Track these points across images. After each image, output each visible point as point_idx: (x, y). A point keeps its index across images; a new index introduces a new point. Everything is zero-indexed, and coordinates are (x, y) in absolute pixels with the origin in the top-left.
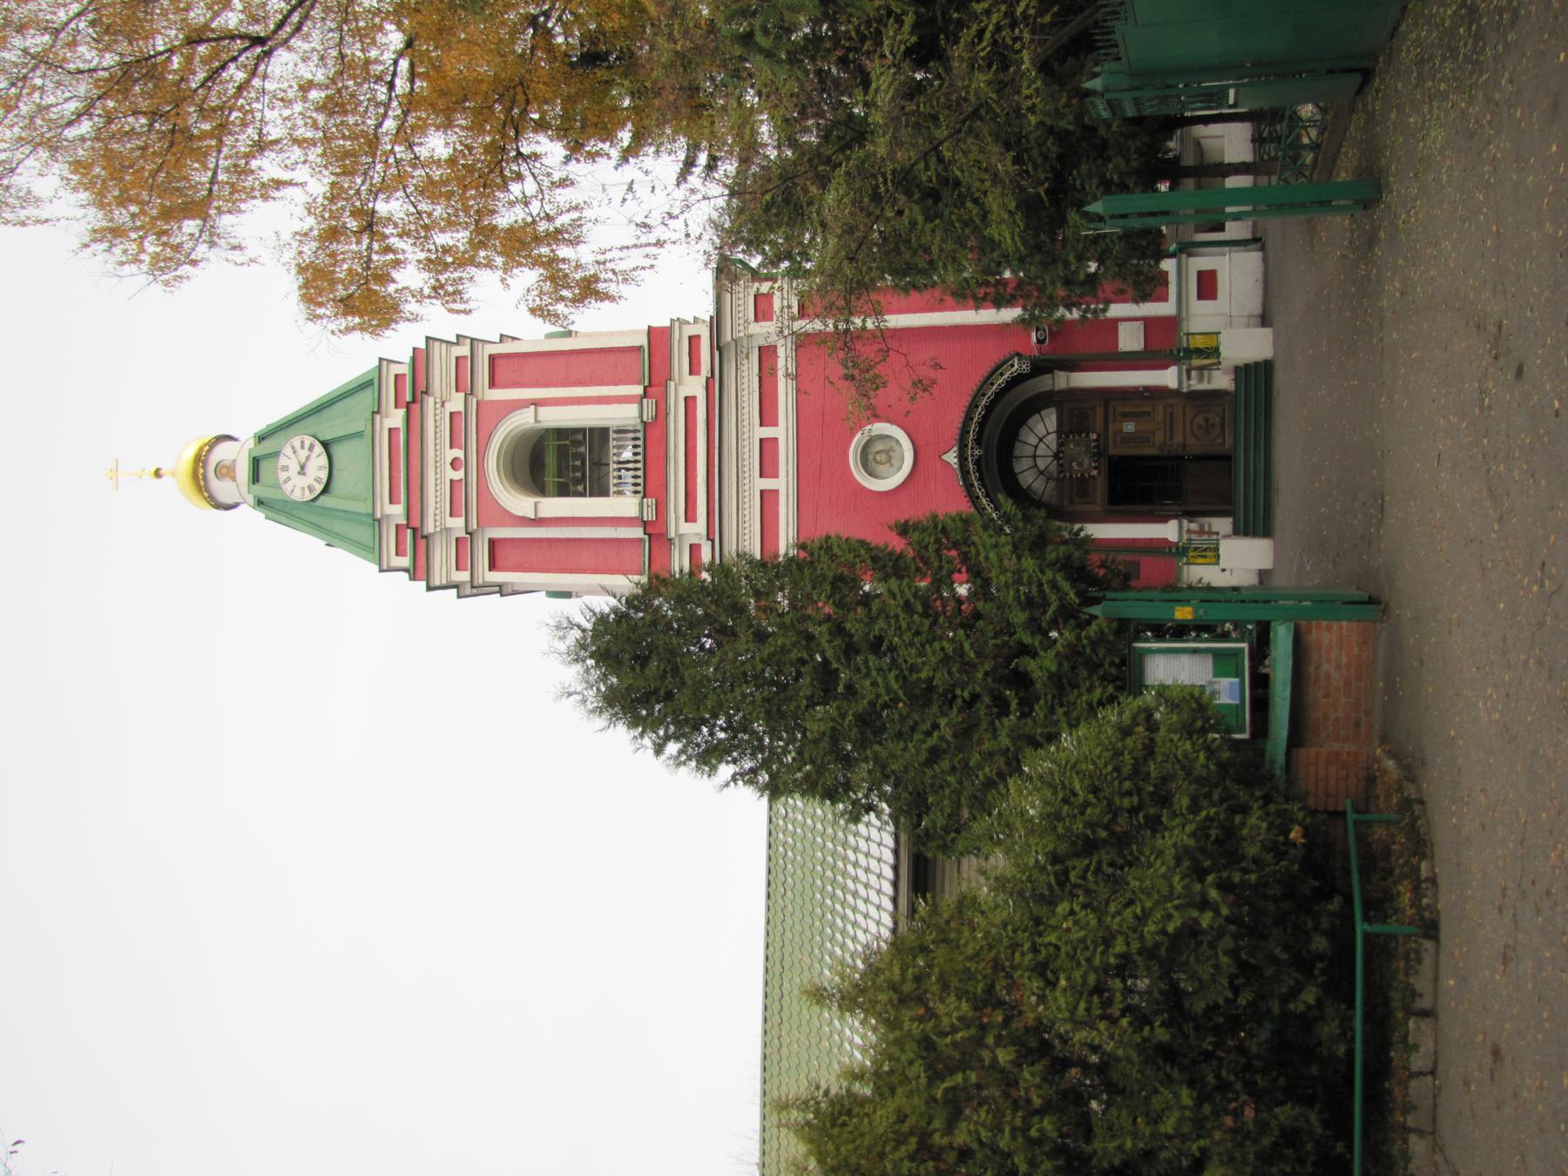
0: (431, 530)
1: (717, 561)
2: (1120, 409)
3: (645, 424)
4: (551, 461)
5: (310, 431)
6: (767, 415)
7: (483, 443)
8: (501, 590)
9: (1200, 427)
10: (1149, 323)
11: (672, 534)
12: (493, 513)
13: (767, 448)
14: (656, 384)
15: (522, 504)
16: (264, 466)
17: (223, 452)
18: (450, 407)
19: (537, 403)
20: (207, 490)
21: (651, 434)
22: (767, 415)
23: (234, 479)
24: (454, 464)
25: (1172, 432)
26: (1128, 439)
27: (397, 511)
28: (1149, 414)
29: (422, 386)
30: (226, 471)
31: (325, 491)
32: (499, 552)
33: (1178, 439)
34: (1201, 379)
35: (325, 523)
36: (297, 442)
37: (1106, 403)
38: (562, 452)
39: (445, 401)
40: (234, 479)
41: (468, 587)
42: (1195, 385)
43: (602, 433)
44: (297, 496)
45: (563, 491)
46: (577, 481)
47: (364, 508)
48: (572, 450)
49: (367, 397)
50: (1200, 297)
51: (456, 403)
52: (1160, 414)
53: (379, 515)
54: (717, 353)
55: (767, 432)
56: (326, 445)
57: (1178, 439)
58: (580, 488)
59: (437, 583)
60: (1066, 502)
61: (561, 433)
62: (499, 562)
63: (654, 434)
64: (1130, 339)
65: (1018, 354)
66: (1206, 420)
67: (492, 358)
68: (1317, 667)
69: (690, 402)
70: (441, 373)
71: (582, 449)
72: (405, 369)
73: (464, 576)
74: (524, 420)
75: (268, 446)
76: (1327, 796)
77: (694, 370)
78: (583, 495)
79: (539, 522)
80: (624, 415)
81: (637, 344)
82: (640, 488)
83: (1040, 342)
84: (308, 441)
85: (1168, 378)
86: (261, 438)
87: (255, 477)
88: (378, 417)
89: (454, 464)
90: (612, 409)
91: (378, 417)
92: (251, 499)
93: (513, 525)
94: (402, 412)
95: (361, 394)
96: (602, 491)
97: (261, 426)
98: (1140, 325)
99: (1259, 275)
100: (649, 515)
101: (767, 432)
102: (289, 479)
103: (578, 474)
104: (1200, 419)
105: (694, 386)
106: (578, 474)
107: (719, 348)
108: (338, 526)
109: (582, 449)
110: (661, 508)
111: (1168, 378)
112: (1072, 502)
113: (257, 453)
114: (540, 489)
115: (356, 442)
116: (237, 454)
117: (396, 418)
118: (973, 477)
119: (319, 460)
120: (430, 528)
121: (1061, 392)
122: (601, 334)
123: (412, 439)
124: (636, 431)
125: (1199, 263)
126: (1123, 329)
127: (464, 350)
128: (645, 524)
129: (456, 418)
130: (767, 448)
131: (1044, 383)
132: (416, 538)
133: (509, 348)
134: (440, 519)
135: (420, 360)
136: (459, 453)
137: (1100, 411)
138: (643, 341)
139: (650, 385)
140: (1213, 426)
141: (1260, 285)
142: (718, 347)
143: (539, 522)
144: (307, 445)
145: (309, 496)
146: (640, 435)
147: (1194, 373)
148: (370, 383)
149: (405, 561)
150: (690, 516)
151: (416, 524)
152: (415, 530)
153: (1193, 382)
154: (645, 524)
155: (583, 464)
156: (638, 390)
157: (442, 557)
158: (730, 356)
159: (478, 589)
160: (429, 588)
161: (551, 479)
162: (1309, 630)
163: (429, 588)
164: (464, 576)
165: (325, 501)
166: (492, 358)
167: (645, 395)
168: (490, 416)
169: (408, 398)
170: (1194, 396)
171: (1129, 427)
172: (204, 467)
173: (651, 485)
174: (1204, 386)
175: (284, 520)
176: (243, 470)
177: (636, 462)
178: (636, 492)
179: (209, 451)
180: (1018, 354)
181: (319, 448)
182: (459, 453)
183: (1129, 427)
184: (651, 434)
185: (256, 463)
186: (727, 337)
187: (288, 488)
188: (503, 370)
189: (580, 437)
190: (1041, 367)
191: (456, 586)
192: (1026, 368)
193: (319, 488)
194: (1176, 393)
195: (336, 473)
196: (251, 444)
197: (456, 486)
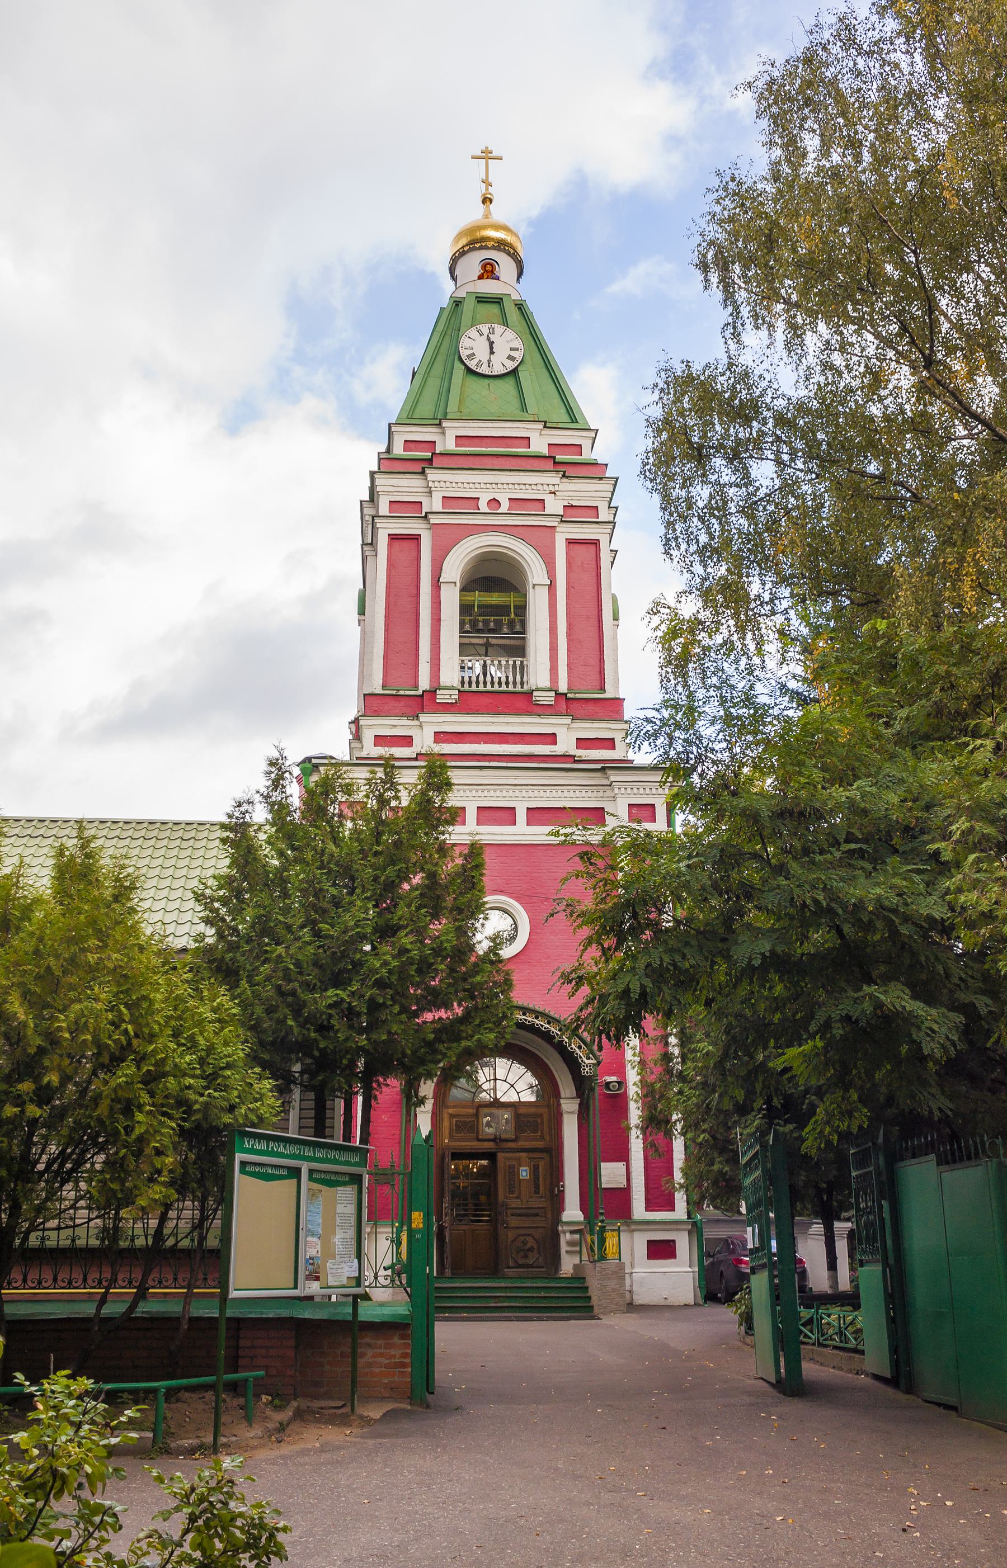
0: (430, 477)
1: (397, 764)
2: (542, 1165)
3: (530, 694)
4: (495, 598)
5: (527, 358)
6: (537, 815)
7: (514, 530)
8: (369, 545)
9: (525, 1243)
10: (624, 1194)
11: (423, 718)
12: (447, 539)
13: (506, 815)
14: (566, 704)
15: (456, 566)
16: (494, 309)
17: (506, 267)
18: (549, 499)
19: (552, 586)
20: (471, 250)
21: (522, 702)
22: (537, 815)
23: (480, 277)
24: (494, 502)
25: (520, 1215)
26: (512, 1173)
27: (447, 443)
28: (537, 1192)
29: (570, 471)
30: (489, 271)
31: (469, 371)
32: (407, 545)
33: (513, 1221)
34: (570, 1243)
35: (438, 368)
36: (518, 344)
37: (546, 1150)
38: (502, 610)
39: (556, 493)
40: (480, 277)
41: (373, 512)
42: (565, 1238)
43: (520, 650)
44: (465, 342)
45: (465, 609)
46: (474, 624)
47: (452, 407)
48: (505, 620)
49: (560, 415)
50: (437, 734)
51: (554, 506)
52: (537, 1203)
53: (445, 424)
54: (599, 766)
55: (521, 816)
56: (514, 372)
57: (513, 1221)
58: (467, 627)
59: (377, 482)
60: (451, 1111)
61: (522, 609)
62: (397, 544)
63: (521, 704)
64: (611, 1174)
65: (599, 1063)
66: (531, 1249)
67: (596, 543)
68: (369, 1345)
69: (551, 738)
70: (581, 491)
71: (505, 630)
72: (586, 455)
73: (384, 509)
74: (536, 572)
75: (513, 314)
76: (252, 1358)
77: (582, 743)
78: (462, 630)
79: (436, 585)
80: (538, 675)
81: (608, 687)
82: (466, 687)
83: (608, 1084)
84: (518, 355)
85: (572, 1212)
86: (520, 306)
87: (482, 299)
88: (541, 426)
89: (494, 502)
90: (544, 662)
91: (541, 426)
92: (461, 294)
93: (433, 560)
94: (545, 451)
95: (563, 410)
96: (464, 649)
97: (533, 307)
98: (622, 1183)
99: (672, 1301)
100: (442, 697)
101: (521, 816)
102: (512, 349)
103: (481, 625)
104: (531, 1243)
105: (565, 744)
106: (481, 625)
107: (603, 769)
108: (434, 383)
109: (505, 630)
110: (447, 708)
111: (572, 1212)
112: (451, 1116)
113: (506, 303)
114: (466, 589)
115: (516, 403)
116: (505, 283)
117: (539, 445)
118: (530, 1019)
119: (500, 365)
120: (432, 475)
121: (559, 1105)
122: (615, 650)
123: (510, 457)
124: (522, 684)
125: (683, 1243)
126: (621, 1166)
127: (604, 515)
128: (432, 692)
129: (539, 505)
130: (506, 815)
131: (567, 1089)
132: (424, 461)
133: (605, 558)
134: (446, 482)
135: (594, 470)
136: (504, 507)
137: (540, 1144)
138: (608, 695)
139: (568, 699)
140: (526, 1256)
141: (663, 1303)
142: (604, 768)
143: (436, 585)
144: (514, 354)
145: (464, 353)
146: (518, 688)
147: (577, 1236)
148: (574, 419)
149: (398, 450)
150: (440, 737)
151: (436, 462)
152: (430, 461)
153: (568, 1236)
154: (432, 692)
155: (490, 631)
156: (563, 688)
157: (406, 487)
158: (597, 779)
159: (369, 523)
160: (372, 474)
161: (478, 598)
162: (403, 1337)
163: (372, 474)
164: (384, 509)
165: (459, 370)
166: (596, 543)
167: (558, 694)
168: (540, 537)
169: (559, 458)
170: (555, 1237)
171: (524, 1173)
172: (493, 248)
173: (469, 700)
174: (564, 1247)
175: (441, 327)
176: (488, 287)
177: (492, 683)
178: (463, 683)
179: (509, 254)
180: (599, 1063)
181: (511, 365)
182: (504, 507)
183: (524, 1173)
184: (522, 702)
185: (497, 301)
186: (614, 777)
187: (473, 333)
188: (584, 553)
189: (518, 628)
190: (582, 1085)
191: (372, 500)
192: (586, 1071)
193: (472, 364)
194: (557, 1220)
195: (486, 381)
196: (515, 296)
197: (473, 503)
